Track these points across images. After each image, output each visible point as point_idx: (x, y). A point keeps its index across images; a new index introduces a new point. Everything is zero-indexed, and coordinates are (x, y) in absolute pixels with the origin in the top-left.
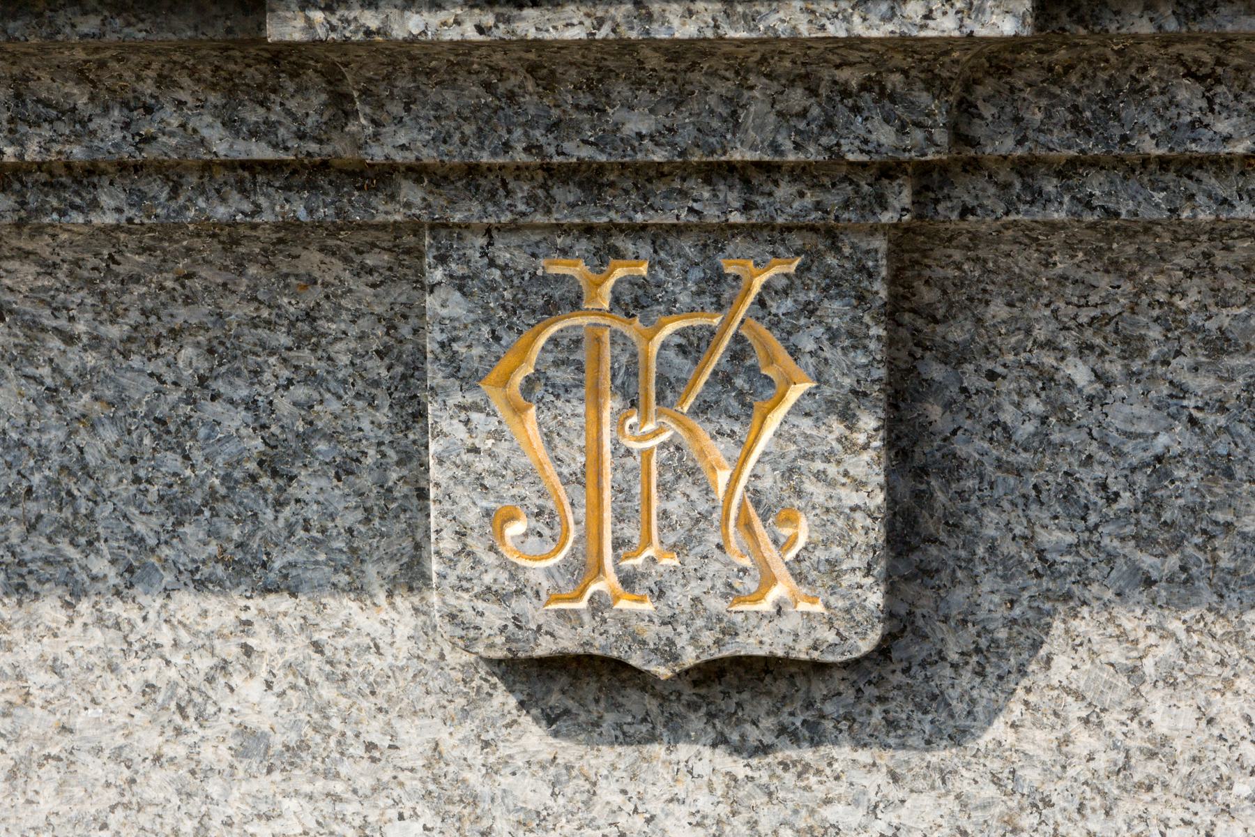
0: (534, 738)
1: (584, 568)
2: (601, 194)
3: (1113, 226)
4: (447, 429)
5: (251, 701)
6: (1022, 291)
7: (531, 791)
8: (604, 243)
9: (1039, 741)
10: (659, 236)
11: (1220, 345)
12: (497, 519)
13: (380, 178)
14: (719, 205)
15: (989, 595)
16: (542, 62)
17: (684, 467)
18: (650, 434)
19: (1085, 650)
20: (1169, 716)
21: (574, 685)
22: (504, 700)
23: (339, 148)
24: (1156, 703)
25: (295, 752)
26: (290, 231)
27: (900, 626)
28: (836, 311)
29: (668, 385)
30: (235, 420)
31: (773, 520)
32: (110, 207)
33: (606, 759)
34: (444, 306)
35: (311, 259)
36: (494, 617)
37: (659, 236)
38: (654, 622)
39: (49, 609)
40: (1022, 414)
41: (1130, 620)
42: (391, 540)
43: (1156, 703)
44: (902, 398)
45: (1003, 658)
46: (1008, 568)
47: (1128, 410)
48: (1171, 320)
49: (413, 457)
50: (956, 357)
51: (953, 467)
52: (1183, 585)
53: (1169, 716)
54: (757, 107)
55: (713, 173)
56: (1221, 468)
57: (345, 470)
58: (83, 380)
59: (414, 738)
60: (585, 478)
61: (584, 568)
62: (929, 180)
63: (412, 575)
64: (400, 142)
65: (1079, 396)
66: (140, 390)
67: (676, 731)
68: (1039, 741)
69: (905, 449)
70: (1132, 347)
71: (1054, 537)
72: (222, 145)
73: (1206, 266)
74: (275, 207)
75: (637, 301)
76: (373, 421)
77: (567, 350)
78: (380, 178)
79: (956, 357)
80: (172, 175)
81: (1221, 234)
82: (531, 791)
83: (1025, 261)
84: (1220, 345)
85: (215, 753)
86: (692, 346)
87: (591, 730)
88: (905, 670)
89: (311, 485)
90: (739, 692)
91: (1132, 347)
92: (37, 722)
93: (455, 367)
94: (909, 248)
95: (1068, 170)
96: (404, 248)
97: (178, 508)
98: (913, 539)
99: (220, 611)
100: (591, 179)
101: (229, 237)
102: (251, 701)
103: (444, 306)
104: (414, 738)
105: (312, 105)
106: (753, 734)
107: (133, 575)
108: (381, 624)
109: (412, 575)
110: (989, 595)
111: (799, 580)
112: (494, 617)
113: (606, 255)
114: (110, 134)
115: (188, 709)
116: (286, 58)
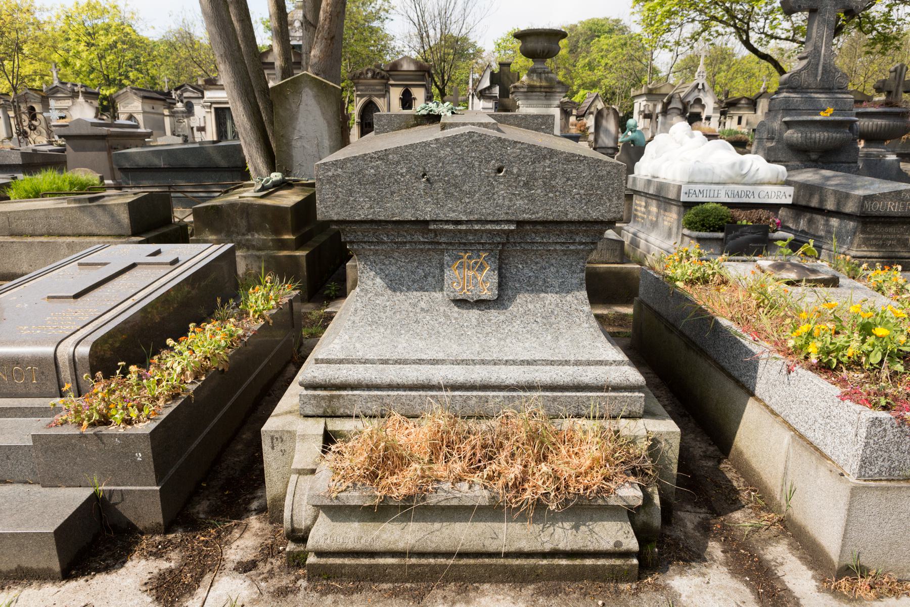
0: (456, 309)
1: (463, 289)
2: (466, 246)
3: (524, 250)
4: (447, 272)
5: (422, 304)
6: (514, 257)
7: (456, 315)
8: (466, 251)
9: (515, 309)
10: (472, 250)
11: (537, 263)
12: (452, 283)
13: (440, 244)
14: (480, 247)
15: (510, 292)
16: (460, 231)
17: (475, 277)
18: (471, 273)
19: (521, 299)
20: (530, 306)
21: (461, 303)
22: (453, 304)
23: (436, 240)
24: (529, 305)
25: (428, 311)
26: (429, 249)
27: (499, 295)
28: (493, 259)
29: (473, 268)
30: (421, 271)
31: (484, 283)
32: (408, 246)
33: (464, 311)
34: (447, 258)
35: (431, 253)
36: (452, 295)
37: (472, 250)
38: (470, 294)
39: (398, 294)
40: (514, 271)
41: (526, 295)
42: (439, 285)
43: (529, 305)
44: (500, 269)
45: (511, 299)
46: (512, 289)
47: (526, 271)
48: (531, 260)
49: (442, 276)
50: (506, 264)
51: (505, 277)
52: (532, 291)
53: (530, 306)
54: (484, 236)
55: (479, 243)
56: (537, 277)
57: (434, 277)
58: (403, 266)
59: (442, 309)
60: (463, 278)
61: (463, 289)
62: (504, 244)
63: (442, 290)
64: (443, 240)
65: (520, 269)
66: (410, 268)
67: (473, 308)
68: (515, 309)
69: (501, 276)
70: (527, 263)
71: (517, 285)
72: (422, 240)
73: (535, 254)
74: (427, 247)
75: (470, 258)
76: (437, 272)
77: (461, 263)
78: (440, 244)
79: (506, 264)
80: (415, 243)
81: (537, 250)
82: (456, 315)
83: (514, 253)
84: (537, 263)
85: (418, 311)
86: (476, 263)
87: (463, 308)
88: (500, 301)
89: (429, 279)
90: (481, 304)
91: (527, 263)
92: (397, 307)
93: (448, 265)
94: (501, 252)
95: (519, 243)
96: (442, 251)
97: (414, 282)
98: (501, 286)
99: (419, 294)
100: (465, 244)
101: (422, 250)
102: (422, 304)
103: (447, 258)
104: (442, 309)
105: (432, 235)
106: (825, 268)
107: (408, 290)
108: (438, 295)
109: (442, 290)
110: (510, 292)
111: (488, 291)
112: (452, 295)
113: (466, 252)
114: (409, 238)
115: (415, 305)
116: (431, 230)
